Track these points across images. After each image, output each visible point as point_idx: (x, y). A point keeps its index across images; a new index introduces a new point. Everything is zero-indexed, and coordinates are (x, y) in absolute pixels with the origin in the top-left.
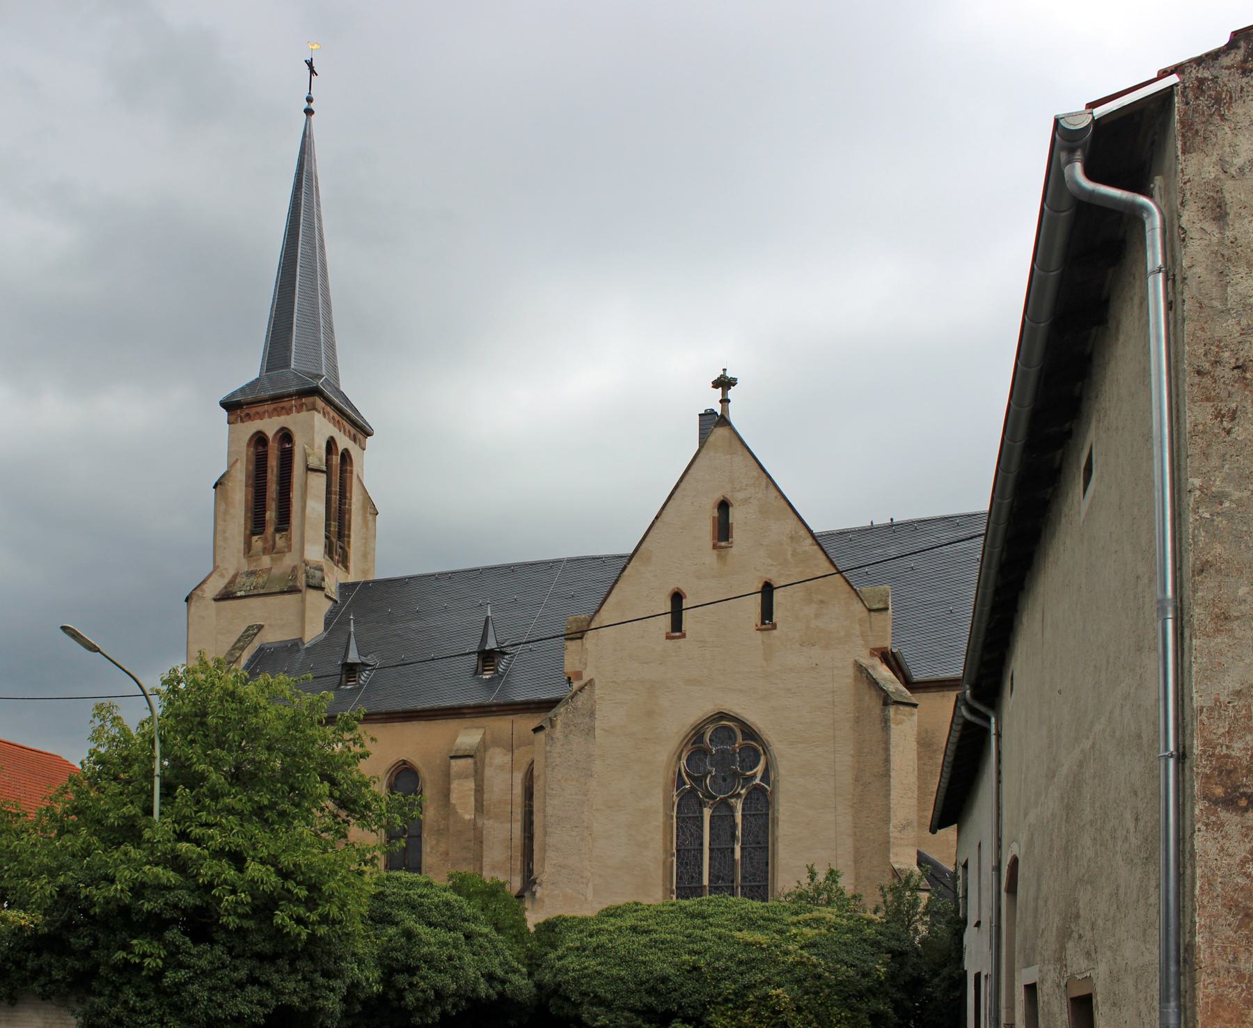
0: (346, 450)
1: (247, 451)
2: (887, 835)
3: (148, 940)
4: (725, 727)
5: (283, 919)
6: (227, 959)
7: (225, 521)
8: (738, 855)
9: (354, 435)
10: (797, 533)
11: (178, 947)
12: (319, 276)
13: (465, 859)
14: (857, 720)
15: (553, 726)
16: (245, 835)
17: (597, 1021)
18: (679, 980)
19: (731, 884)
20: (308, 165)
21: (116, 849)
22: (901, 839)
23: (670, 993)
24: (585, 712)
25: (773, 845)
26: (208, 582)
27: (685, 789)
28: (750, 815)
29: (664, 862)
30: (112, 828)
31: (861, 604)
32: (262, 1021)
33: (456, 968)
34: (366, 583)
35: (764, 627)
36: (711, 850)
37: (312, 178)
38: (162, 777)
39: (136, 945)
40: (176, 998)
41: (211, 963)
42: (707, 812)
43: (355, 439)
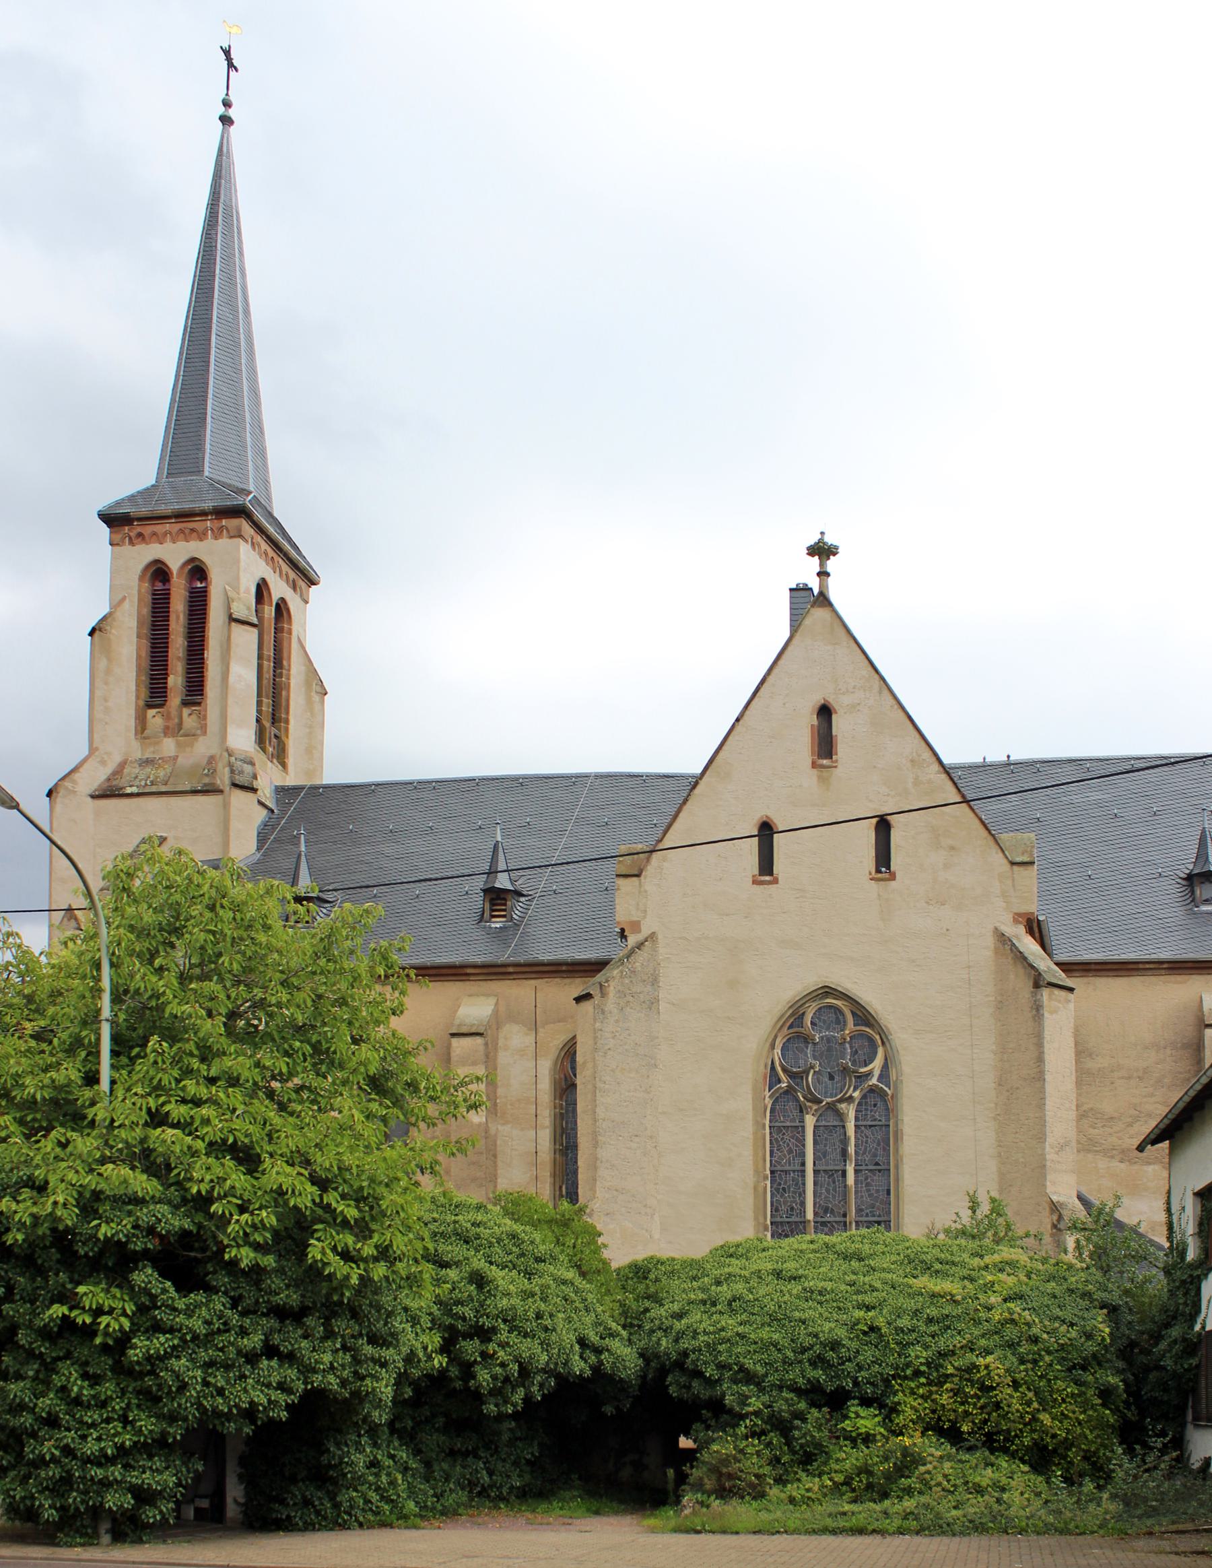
0: (283, 599)
1: (139, 586)
2: (1043, 1156)
3: (103, 1286)
4: (830, 1007)
5: (323, 1253)
6: (235, 1319)
7: (106, 683)
8: (851, 1179)
9: (294, 581)
10: (919, 756)
11: (153, 1298)
12: (243, 352)
13: (474, 1180)
14: (1000, 1006)
15: (603, 994)
16: (255, 1119)
17: (749, 1405)
18: (854, 1345)
19: (842, 1219)
20: (225, 195)
21: (44, 1136)
22: (1059, 1162)
23: (843, 1364)
24: (645, 978)
25: (897, 1167)
26: (81, 770)
27: (780, 1088)
28: (865, 1126)
29: (755, 1188)
30: (31, 1104)
31: (1001, 855)
32: (284, 1415)
33: (546, 1329)
34: (315, 788)
35: (879, 875)
36: (816, 1172)
37: (232, 215)
38: (113, 1023)
39: (85, 1294)
40: (149, 1381)
41: (208, 1323)
42: (810, 1121)
43: (294, 587)
